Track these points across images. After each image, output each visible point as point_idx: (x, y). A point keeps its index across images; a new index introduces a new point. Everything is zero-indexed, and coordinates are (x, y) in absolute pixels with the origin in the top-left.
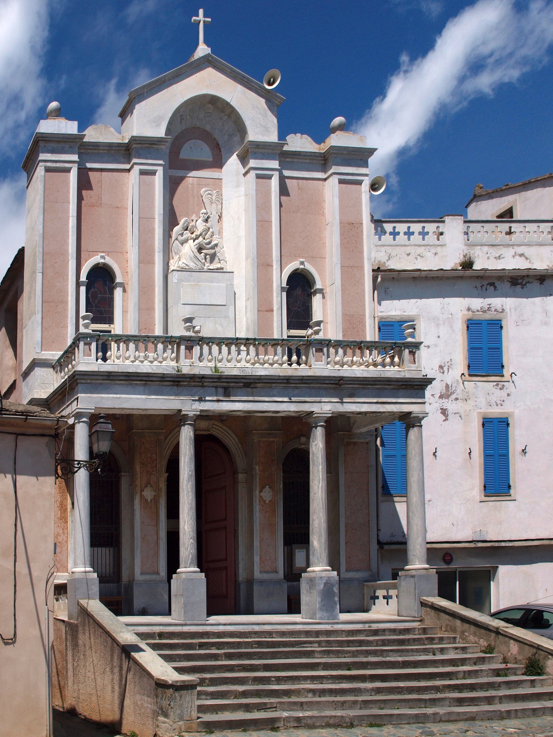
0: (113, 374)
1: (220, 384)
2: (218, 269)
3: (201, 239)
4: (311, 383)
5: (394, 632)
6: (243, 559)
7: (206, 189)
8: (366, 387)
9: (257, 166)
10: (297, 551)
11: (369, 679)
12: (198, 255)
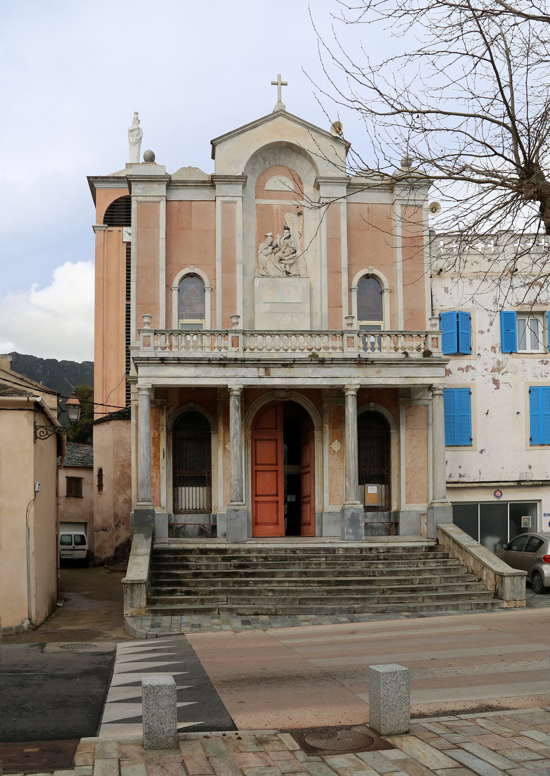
6: (319, 495)
7: (289, 214)
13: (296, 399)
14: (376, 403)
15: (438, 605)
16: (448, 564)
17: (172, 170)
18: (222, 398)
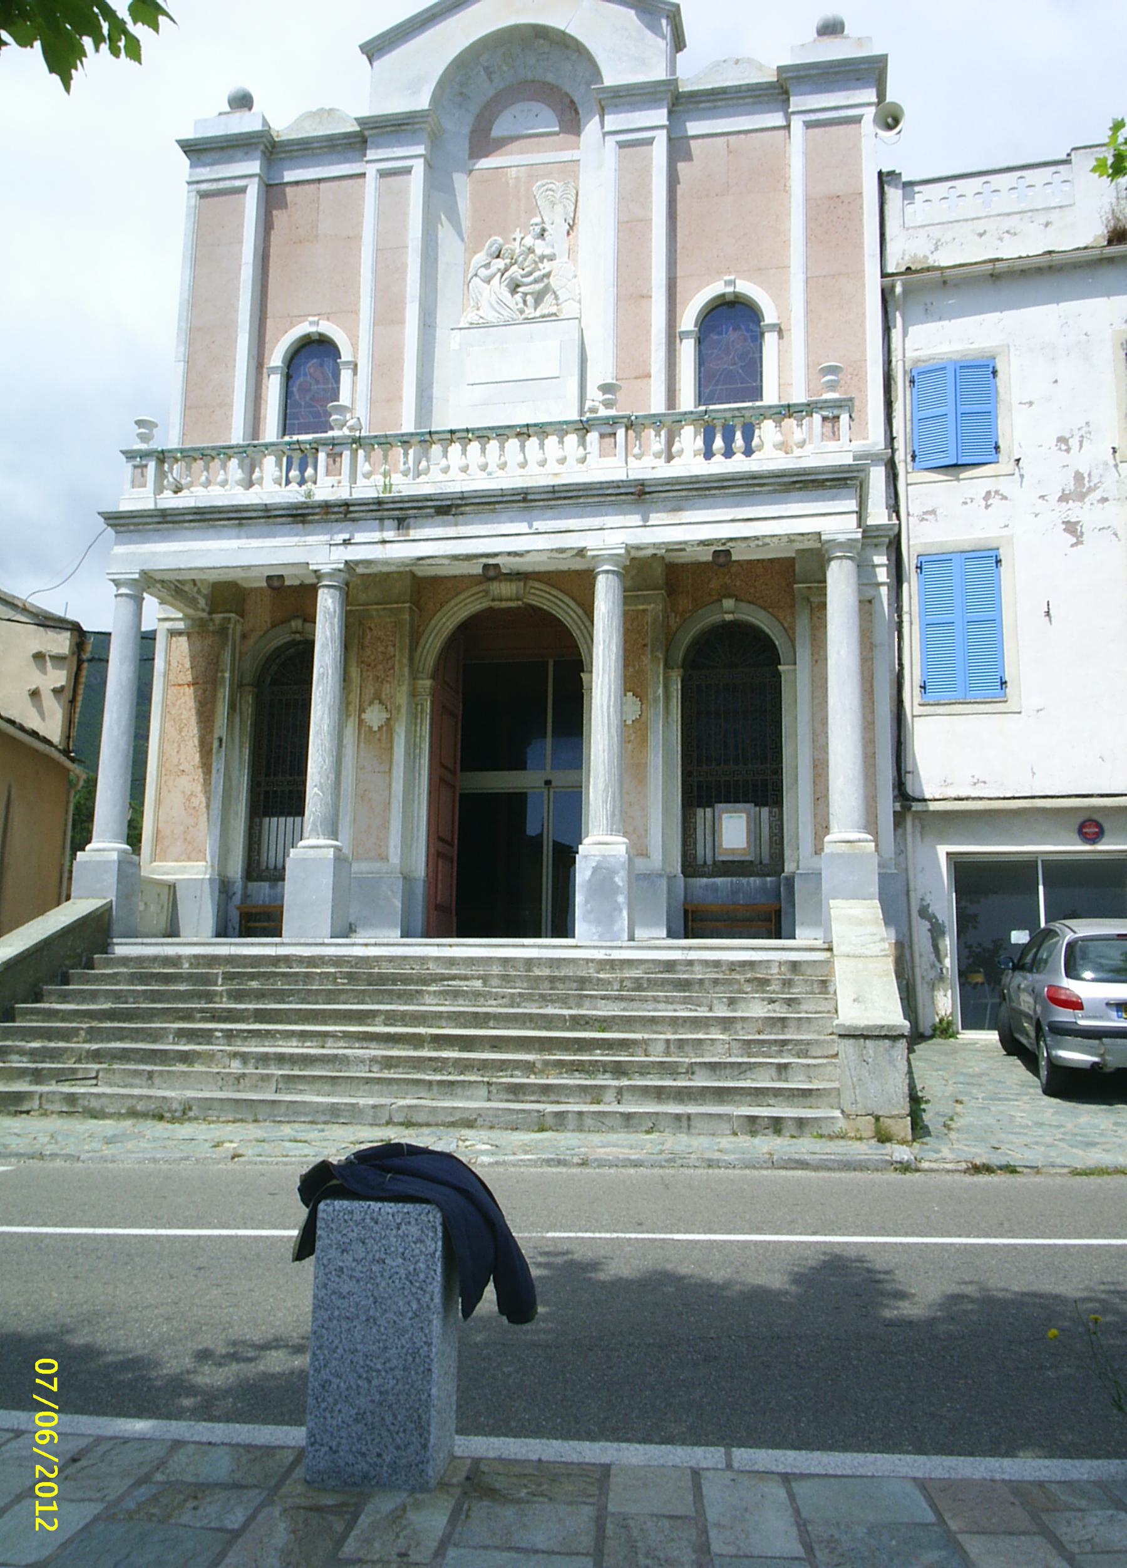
0: (169, 512)
1: (386, 513)
2: (543, 316)
3: (515, 268)
4: (580, 497)
5: (716, 967)
8: (707, 492)
9: (618, 129)
10: (725, 816)
11: (429, 1043)
12: (506, 294)
13: (541, 600)
14: (738, 599)
15: (629, 1114)
16: (804, 1007)
17: (284, 126)
18: (359, 605)
